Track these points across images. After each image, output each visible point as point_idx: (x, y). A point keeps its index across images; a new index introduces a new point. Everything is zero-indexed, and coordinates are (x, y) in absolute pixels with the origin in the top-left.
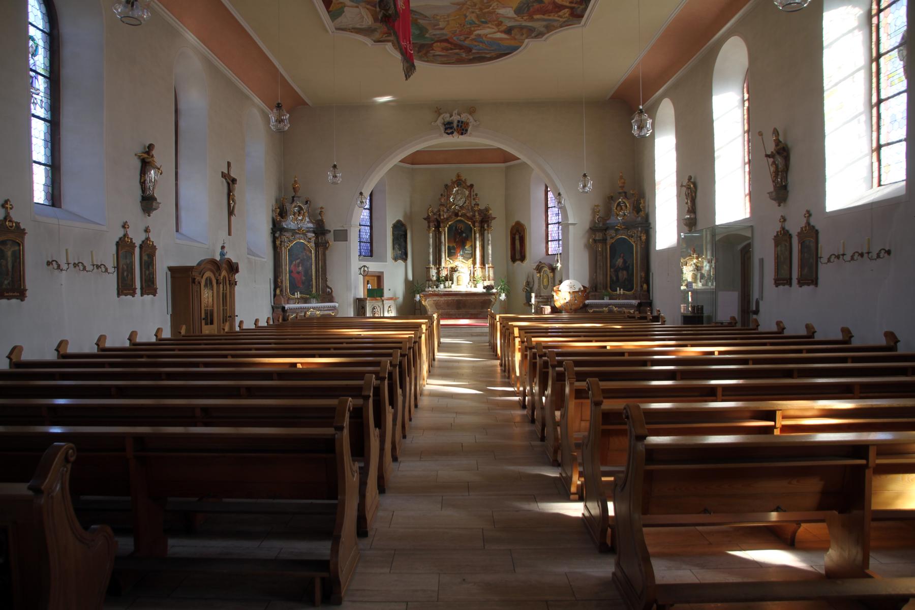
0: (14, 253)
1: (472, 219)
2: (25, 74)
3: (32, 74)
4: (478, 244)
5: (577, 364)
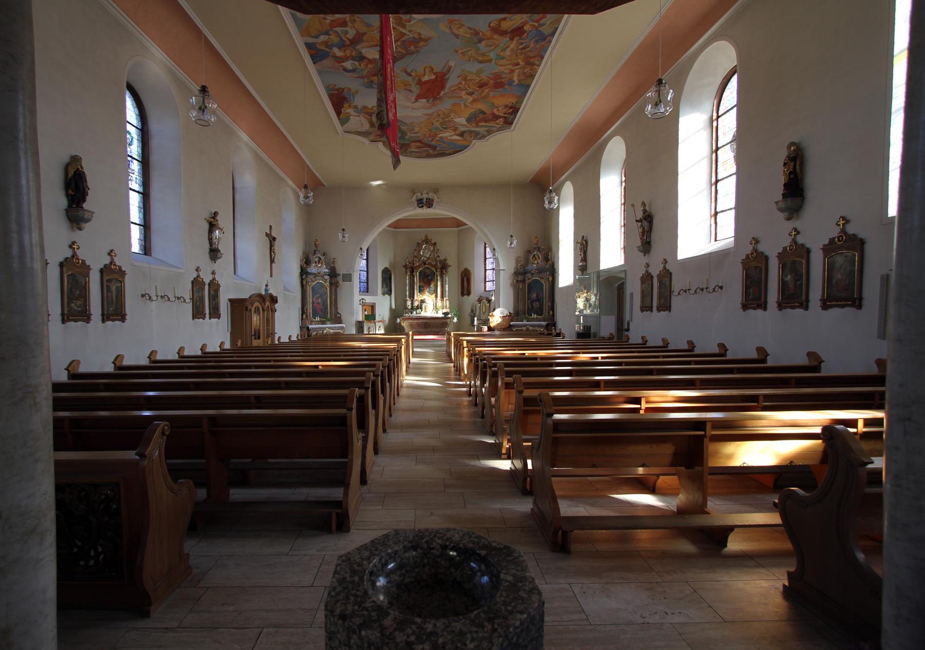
0: (117, 288)
1: (435, 266)
2: (125, 159)
3: (129, 159)
4: (439, 284)
5: (506, 365)
